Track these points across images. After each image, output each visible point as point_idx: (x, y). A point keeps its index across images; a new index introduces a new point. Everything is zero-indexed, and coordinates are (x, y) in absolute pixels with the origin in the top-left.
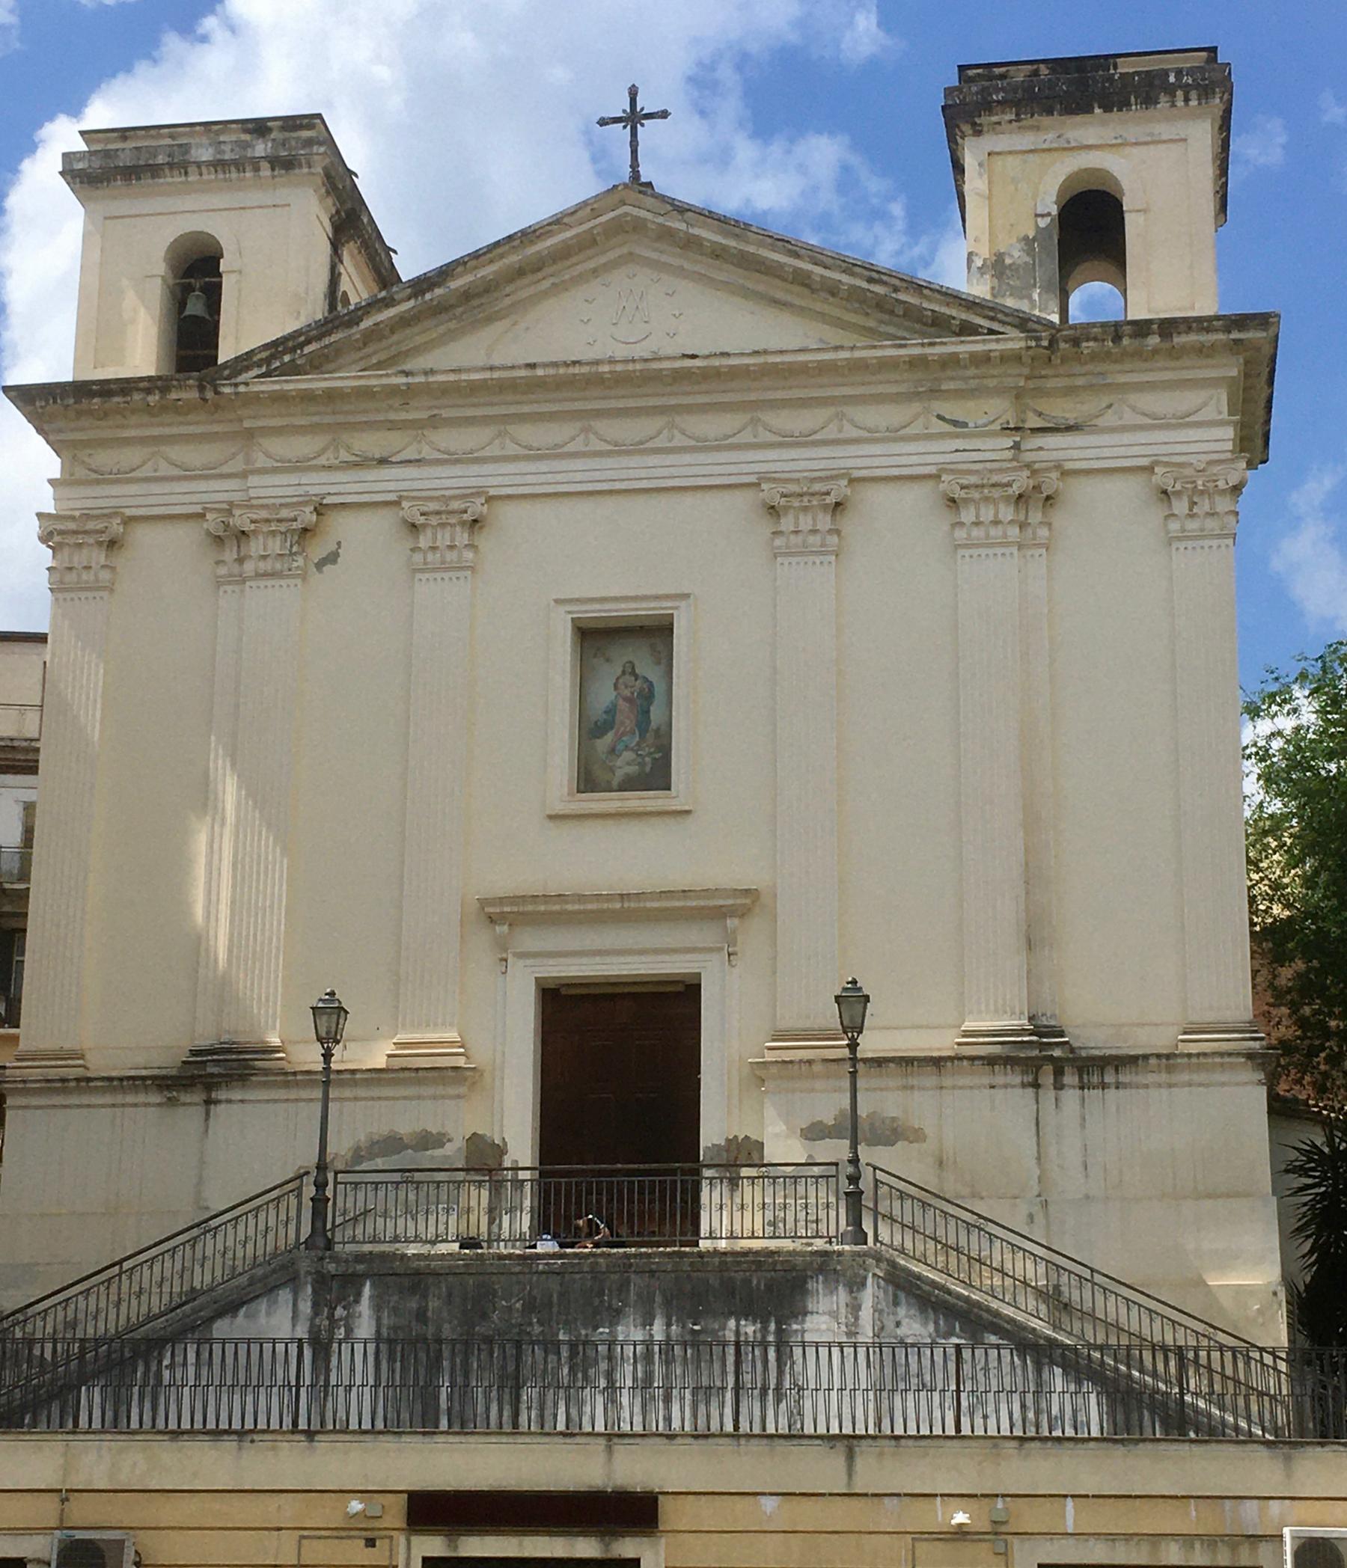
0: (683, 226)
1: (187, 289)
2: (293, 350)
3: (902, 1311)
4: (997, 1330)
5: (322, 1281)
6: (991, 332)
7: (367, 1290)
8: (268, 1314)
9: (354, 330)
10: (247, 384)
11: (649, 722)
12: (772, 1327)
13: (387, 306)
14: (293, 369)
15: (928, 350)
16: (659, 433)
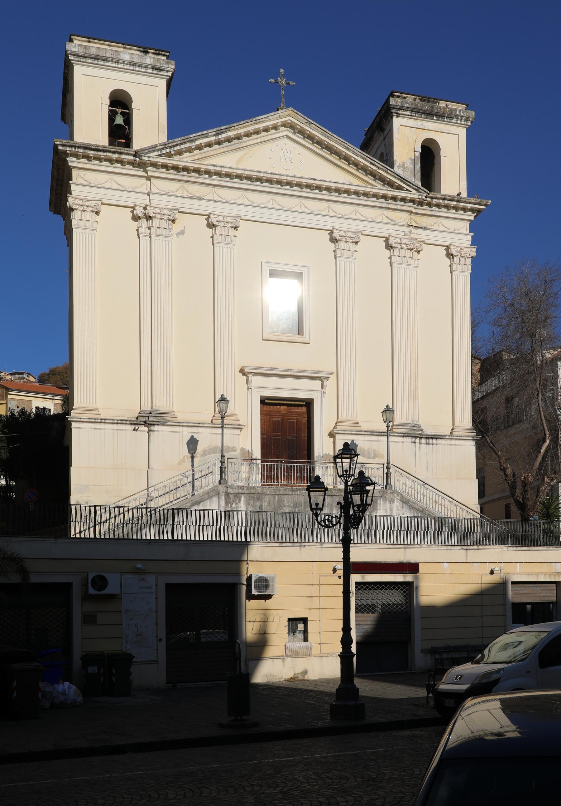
0: (309, 129)
2: (171, 147)
3: (404, 509)
5: (227, 495)
6: (407, 190)
7: (243, 498)
9: (193, 144)
10: (153, 157)
13: (206, 137)
14: (169, 155)
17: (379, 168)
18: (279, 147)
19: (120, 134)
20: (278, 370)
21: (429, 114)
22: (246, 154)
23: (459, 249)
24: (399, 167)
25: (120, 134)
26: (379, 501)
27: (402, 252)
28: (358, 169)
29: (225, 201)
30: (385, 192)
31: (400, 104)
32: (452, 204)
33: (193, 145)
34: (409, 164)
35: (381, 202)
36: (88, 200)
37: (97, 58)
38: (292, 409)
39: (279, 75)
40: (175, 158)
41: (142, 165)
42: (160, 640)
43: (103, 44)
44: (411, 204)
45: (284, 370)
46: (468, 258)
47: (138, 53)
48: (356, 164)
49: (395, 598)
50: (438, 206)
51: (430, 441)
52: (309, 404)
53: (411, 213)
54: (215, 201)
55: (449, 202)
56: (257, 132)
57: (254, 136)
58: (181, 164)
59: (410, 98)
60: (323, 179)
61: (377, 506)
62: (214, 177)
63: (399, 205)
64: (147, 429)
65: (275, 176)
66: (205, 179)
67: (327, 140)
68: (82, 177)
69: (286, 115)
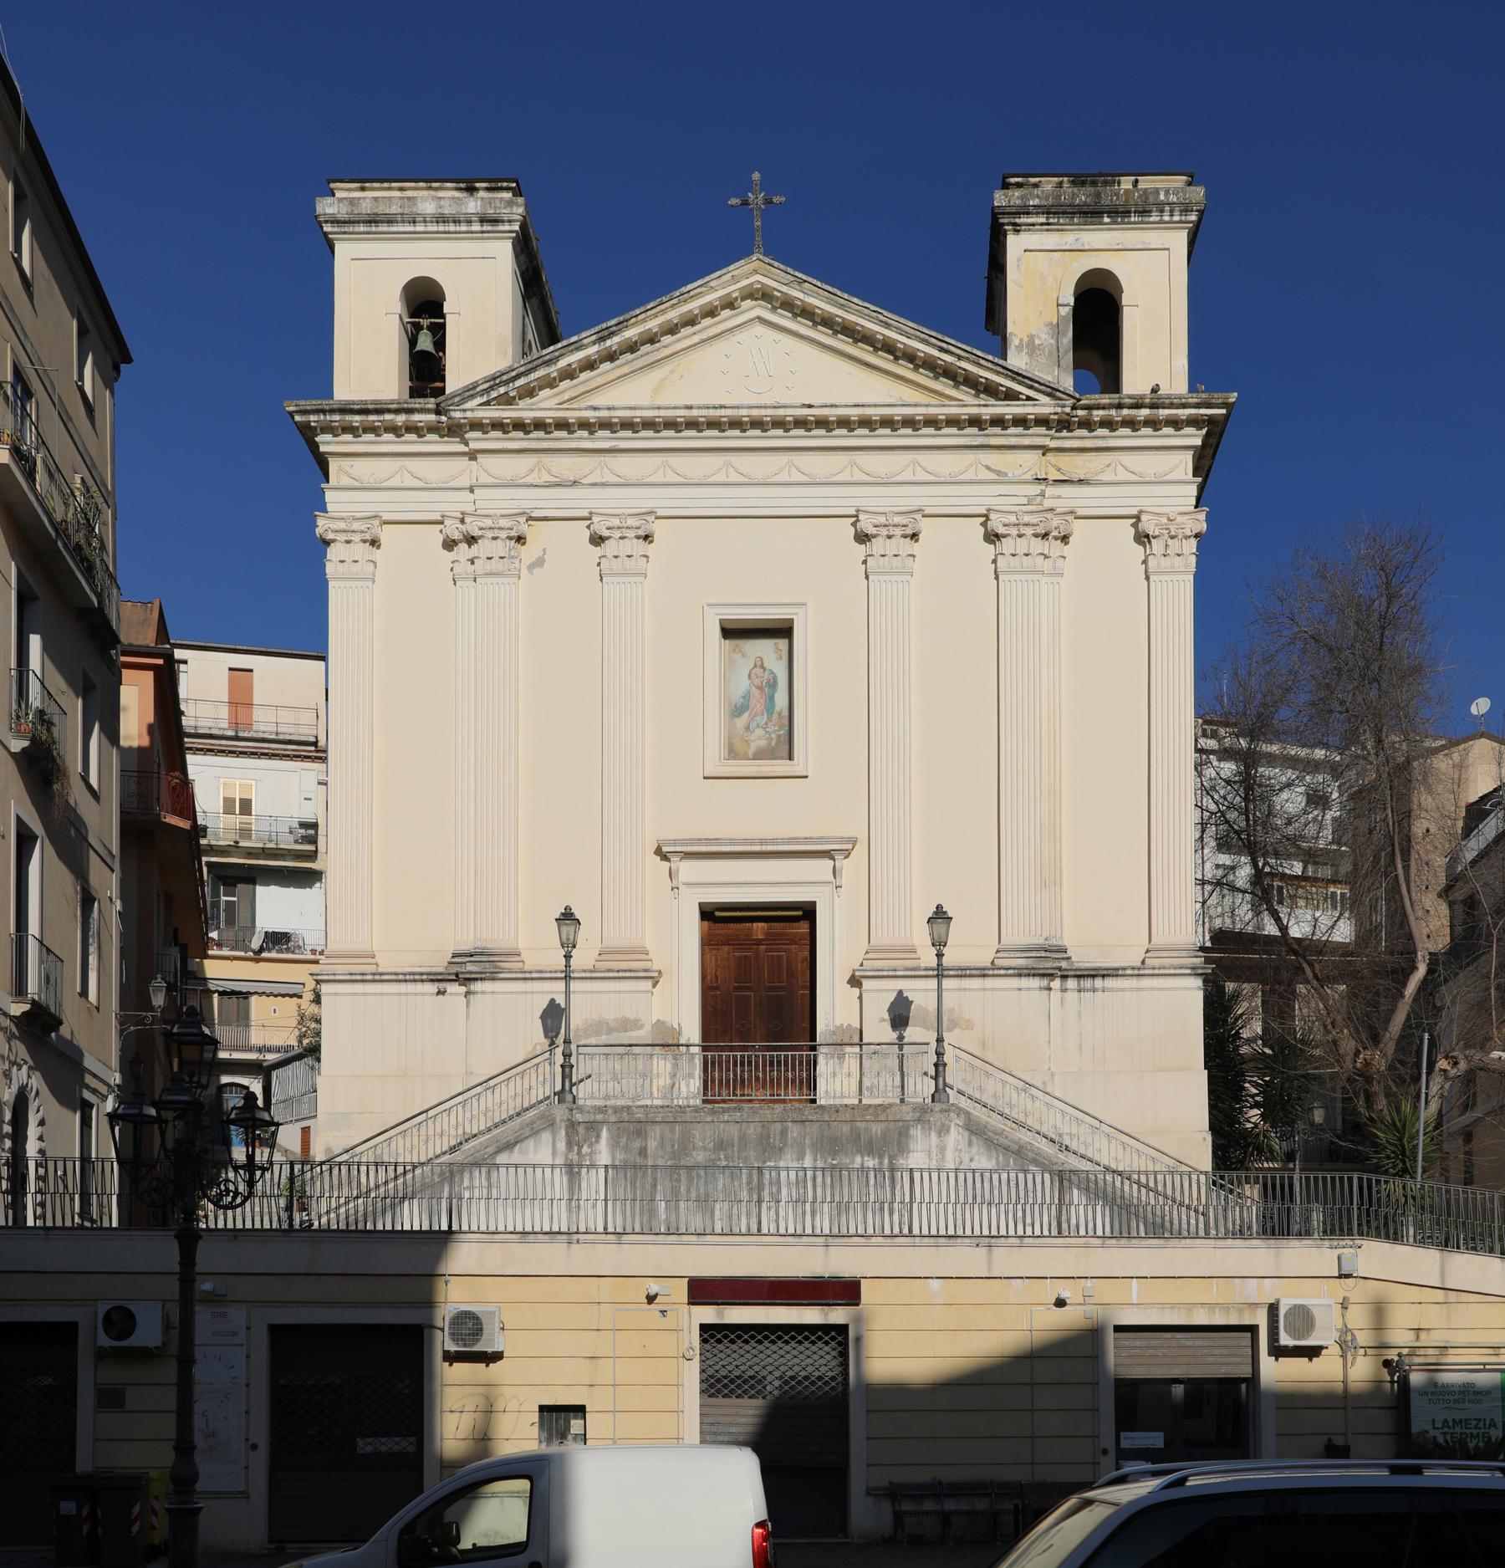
0: (800, 295)
1: (417, 327)
2: (507, 382)
3: (975, 1149)
4: (1035, 1162)
5: (572, 1126)
7: (604, 1133)
8: (535, 1151)
9: (553, 368)
11: (773, 706)
12: (886, 1161)
13: (578, 349)
14: (507, 400)
15: (983, 410)
16: (781, 470)
17: (960, 358)
18: (748, 344)
19: (426, 371)
20: (732, 842)
21: (1091, 214)
22: (671, 372)
23: (1164, 520)
24: (1019, 348)
25: (426, 371)
26: (912, 1132)
27: (1022, 546)
28: (916, 368)
29: (624, 481)
30: (932, 411)
31: (1018, 202)
32: (1153, 413)
33: (553, 371)
34: (1045, 338)
35: (971, 436)
36: (355, 519)
37: (373, 220)
38: (778, 927)
39: (749, 186)
40: (522, 404)
41: (454, 430)
42: (254, 1447)
43: (389, 189)
44: (1042, 430)
45: (745, 841)
46: (1187, 537)
47: (457, 194)
48: (910, 357)
49: (816, 1361)
50: (1108, 424)
51: (1088, 983)
52: (807, 913)
53: (1045, 450)
54: (604, 485)
55: (1133, 412)
56: (691, 321)
57: (685, 331)
58: (528, 416)
59: (1048, 184)
60: (829, 402)
61: (907, 1144)
62: (600, 433)
63: (1014, 435)
64: (463, 989)
65: (723, 412)
66: (581, 439)
67: (840, 312)
68: (346, 473)
69: (751, 271)
